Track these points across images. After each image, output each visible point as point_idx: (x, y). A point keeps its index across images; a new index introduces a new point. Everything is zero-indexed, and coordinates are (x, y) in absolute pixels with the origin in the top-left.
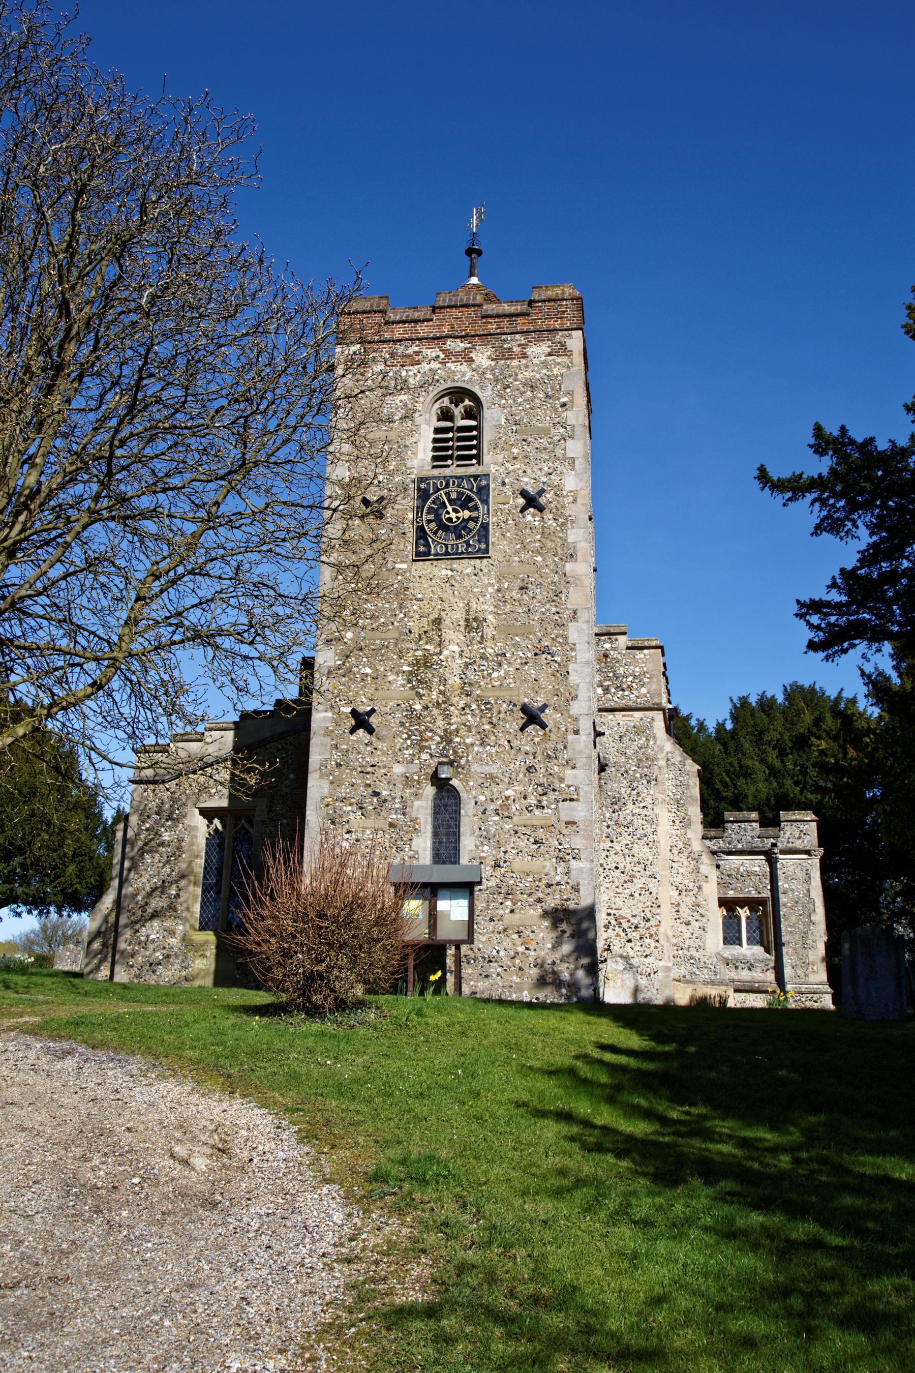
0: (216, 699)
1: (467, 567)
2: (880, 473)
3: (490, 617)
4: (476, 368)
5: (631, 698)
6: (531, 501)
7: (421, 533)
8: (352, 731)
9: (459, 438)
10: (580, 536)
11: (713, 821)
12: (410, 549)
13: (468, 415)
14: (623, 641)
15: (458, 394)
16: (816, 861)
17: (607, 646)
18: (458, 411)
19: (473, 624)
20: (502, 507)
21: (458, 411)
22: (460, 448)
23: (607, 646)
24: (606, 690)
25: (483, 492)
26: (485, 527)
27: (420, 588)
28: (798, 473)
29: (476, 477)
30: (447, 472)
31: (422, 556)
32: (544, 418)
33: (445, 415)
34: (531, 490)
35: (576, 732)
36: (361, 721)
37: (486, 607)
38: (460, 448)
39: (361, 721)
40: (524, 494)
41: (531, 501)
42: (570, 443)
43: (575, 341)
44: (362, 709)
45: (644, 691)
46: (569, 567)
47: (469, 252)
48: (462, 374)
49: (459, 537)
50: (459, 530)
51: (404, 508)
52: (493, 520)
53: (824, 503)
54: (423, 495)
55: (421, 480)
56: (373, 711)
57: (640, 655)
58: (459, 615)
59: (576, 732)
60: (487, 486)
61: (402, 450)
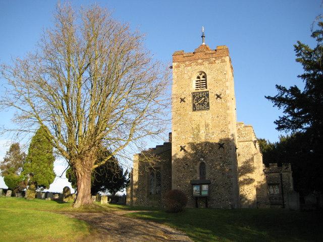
1: (205, 112)
2: (311, 151)
3: (210, 124)
4: (206, 67)
5: (245, 139)
6: (218, 96)
9: (202, 80)
10: (232, 104)
12: (191, 108)
13: (203, 77)
14: (243, 125)
15: (202, 72)
16: (291, 174)
18: (201, 76)
19: (207, 126)
20: (212, 100)
21: (201, 76)
24: (239, 137)
25: (208, 95)
26: (208, 103)
28: (294, 48)
29: (206, 92)
30: (199, 91)
31: (194, 110)
33: (198, 77)
34: (219, 94)
35: (231, 149)
37: (209, 122)
40: (217, 95)
41: (218, 96)
42: (227, 83)
43: (227, 59)
45: (248, 137)
46: (228, 111)
47: (202, 37)
48: (202, 68)
49: (203, 106)
51: (189, 99)
52: (210, 101)
54: (194, 97)
55: (194, 93)
57: (247, 128)
58: (203, 123)
59: (231, 149)
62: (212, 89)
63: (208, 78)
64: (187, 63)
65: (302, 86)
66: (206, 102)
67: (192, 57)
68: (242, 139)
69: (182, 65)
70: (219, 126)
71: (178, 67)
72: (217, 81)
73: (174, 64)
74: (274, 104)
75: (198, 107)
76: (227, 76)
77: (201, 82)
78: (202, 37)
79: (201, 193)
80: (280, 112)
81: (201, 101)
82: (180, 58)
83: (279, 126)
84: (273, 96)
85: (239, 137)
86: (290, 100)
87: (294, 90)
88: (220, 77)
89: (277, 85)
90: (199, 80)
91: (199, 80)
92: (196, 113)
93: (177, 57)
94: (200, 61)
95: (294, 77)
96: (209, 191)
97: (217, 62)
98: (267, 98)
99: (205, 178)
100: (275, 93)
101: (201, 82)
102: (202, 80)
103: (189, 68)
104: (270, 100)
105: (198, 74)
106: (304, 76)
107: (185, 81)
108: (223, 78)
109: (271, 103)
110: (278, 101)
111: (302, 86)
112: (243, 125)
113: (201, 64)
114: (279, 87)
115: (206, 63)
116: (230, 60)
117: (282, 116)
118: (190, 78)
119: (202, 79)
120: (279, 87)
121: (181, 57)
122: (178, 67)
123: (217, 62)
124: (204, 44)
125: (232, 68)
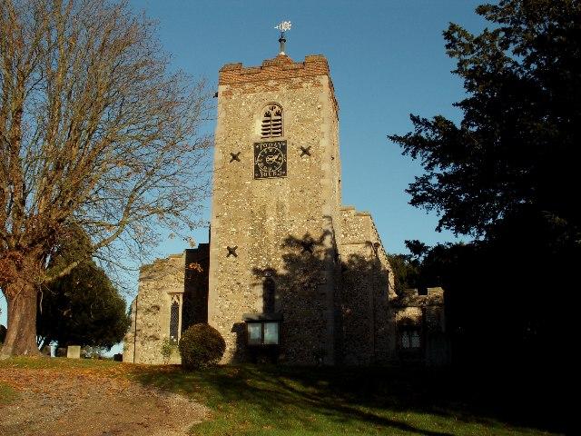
0: (172, 245)
1: (277, 181)
4: (281, 95)
6: (305, 151)
7: (257, 168)
8: (228, 256)
9: (273, 122)
11: (435, 118)
15: (273, 105)
17: (346, 215)
19: (280, 207)
20: (293, 158)
21: (273, 113)
22: (274, 125)
23: (346, 215)
24: (346, 235)
25: (284, 149)
26: (285, 163)
27: (256, 192)
30: (268, 140)
32: (311, 114)
33: (268, 115)
34: (305, 147)
36: (231, 251)
38: (274, 125)
39: (231, 251)
40: (302, 148)
41: (305, 151)
43: (324, 80)
44: (232, 247)
46: (322, 181)
47: (280, 40)
48: (276, 97)
50: (274, 165)
53: (450, 225)
54: (257, 151)
55: (256, 144)
56: (236, 247)
60: (286, 146)
61: (248, 129)
62: (294, 137)
63: (287, 116)
64: (247, 86)
65: (457, 117)
66: (281, 161)
67: (256, 75)
68: (350, 238)
69: (237, 92)
70: (303, 209)
71: (228, 93)
72: (302, 121)
73: (222, 89)
74: (403, 149)
75: (263, 170)
76: (322, 113)
77: (273, 123)
78: (280, 40)
79: (411, 345)
80: (414, 167)
81: (270, 160)
82: (234, 76)
83: (416, 197)
84: (402, 135)
85: (346, 235)
86: (434, 141)
87: (440, 124)
88: (311, 114)
89: (411, 115)
90: (268, 118)
91: (268, 118)
92: (258, 182)
93: (229, 74)
94: (271, 83)
95: (445, 96)
96: (282, 334)
97: (304, 85)
98: (391, 138)
99: (274, 309)
100: (409, 128)
101: (273, 123)
102: (273, 122)
103: (249, 96)
104: (397, 145)
105: (267, 108)
106: (465, 104)
107: (238, 120)
108: (310, 116)
109: (398, 148)
110: (413, 144)
111: (457, 117)
112: (353, 212)
113: (274, 89)
114: (415, 120)
115: (283, 89)
116: (331, 85)
117: (420, 176)
118: (251, 115)
119: (274, 117)
120: (415, 120)
121: (240, 75)
122: (228, 93)
123: (304, 85)
124: (283, 53)
125: (336, 103)
